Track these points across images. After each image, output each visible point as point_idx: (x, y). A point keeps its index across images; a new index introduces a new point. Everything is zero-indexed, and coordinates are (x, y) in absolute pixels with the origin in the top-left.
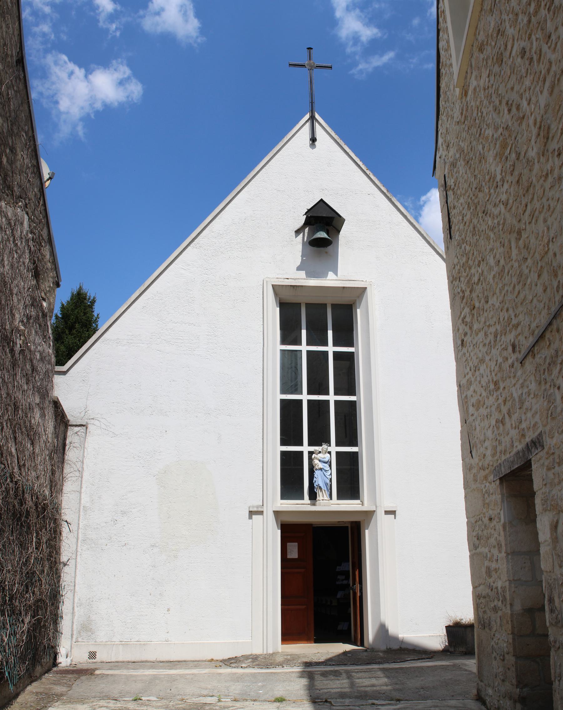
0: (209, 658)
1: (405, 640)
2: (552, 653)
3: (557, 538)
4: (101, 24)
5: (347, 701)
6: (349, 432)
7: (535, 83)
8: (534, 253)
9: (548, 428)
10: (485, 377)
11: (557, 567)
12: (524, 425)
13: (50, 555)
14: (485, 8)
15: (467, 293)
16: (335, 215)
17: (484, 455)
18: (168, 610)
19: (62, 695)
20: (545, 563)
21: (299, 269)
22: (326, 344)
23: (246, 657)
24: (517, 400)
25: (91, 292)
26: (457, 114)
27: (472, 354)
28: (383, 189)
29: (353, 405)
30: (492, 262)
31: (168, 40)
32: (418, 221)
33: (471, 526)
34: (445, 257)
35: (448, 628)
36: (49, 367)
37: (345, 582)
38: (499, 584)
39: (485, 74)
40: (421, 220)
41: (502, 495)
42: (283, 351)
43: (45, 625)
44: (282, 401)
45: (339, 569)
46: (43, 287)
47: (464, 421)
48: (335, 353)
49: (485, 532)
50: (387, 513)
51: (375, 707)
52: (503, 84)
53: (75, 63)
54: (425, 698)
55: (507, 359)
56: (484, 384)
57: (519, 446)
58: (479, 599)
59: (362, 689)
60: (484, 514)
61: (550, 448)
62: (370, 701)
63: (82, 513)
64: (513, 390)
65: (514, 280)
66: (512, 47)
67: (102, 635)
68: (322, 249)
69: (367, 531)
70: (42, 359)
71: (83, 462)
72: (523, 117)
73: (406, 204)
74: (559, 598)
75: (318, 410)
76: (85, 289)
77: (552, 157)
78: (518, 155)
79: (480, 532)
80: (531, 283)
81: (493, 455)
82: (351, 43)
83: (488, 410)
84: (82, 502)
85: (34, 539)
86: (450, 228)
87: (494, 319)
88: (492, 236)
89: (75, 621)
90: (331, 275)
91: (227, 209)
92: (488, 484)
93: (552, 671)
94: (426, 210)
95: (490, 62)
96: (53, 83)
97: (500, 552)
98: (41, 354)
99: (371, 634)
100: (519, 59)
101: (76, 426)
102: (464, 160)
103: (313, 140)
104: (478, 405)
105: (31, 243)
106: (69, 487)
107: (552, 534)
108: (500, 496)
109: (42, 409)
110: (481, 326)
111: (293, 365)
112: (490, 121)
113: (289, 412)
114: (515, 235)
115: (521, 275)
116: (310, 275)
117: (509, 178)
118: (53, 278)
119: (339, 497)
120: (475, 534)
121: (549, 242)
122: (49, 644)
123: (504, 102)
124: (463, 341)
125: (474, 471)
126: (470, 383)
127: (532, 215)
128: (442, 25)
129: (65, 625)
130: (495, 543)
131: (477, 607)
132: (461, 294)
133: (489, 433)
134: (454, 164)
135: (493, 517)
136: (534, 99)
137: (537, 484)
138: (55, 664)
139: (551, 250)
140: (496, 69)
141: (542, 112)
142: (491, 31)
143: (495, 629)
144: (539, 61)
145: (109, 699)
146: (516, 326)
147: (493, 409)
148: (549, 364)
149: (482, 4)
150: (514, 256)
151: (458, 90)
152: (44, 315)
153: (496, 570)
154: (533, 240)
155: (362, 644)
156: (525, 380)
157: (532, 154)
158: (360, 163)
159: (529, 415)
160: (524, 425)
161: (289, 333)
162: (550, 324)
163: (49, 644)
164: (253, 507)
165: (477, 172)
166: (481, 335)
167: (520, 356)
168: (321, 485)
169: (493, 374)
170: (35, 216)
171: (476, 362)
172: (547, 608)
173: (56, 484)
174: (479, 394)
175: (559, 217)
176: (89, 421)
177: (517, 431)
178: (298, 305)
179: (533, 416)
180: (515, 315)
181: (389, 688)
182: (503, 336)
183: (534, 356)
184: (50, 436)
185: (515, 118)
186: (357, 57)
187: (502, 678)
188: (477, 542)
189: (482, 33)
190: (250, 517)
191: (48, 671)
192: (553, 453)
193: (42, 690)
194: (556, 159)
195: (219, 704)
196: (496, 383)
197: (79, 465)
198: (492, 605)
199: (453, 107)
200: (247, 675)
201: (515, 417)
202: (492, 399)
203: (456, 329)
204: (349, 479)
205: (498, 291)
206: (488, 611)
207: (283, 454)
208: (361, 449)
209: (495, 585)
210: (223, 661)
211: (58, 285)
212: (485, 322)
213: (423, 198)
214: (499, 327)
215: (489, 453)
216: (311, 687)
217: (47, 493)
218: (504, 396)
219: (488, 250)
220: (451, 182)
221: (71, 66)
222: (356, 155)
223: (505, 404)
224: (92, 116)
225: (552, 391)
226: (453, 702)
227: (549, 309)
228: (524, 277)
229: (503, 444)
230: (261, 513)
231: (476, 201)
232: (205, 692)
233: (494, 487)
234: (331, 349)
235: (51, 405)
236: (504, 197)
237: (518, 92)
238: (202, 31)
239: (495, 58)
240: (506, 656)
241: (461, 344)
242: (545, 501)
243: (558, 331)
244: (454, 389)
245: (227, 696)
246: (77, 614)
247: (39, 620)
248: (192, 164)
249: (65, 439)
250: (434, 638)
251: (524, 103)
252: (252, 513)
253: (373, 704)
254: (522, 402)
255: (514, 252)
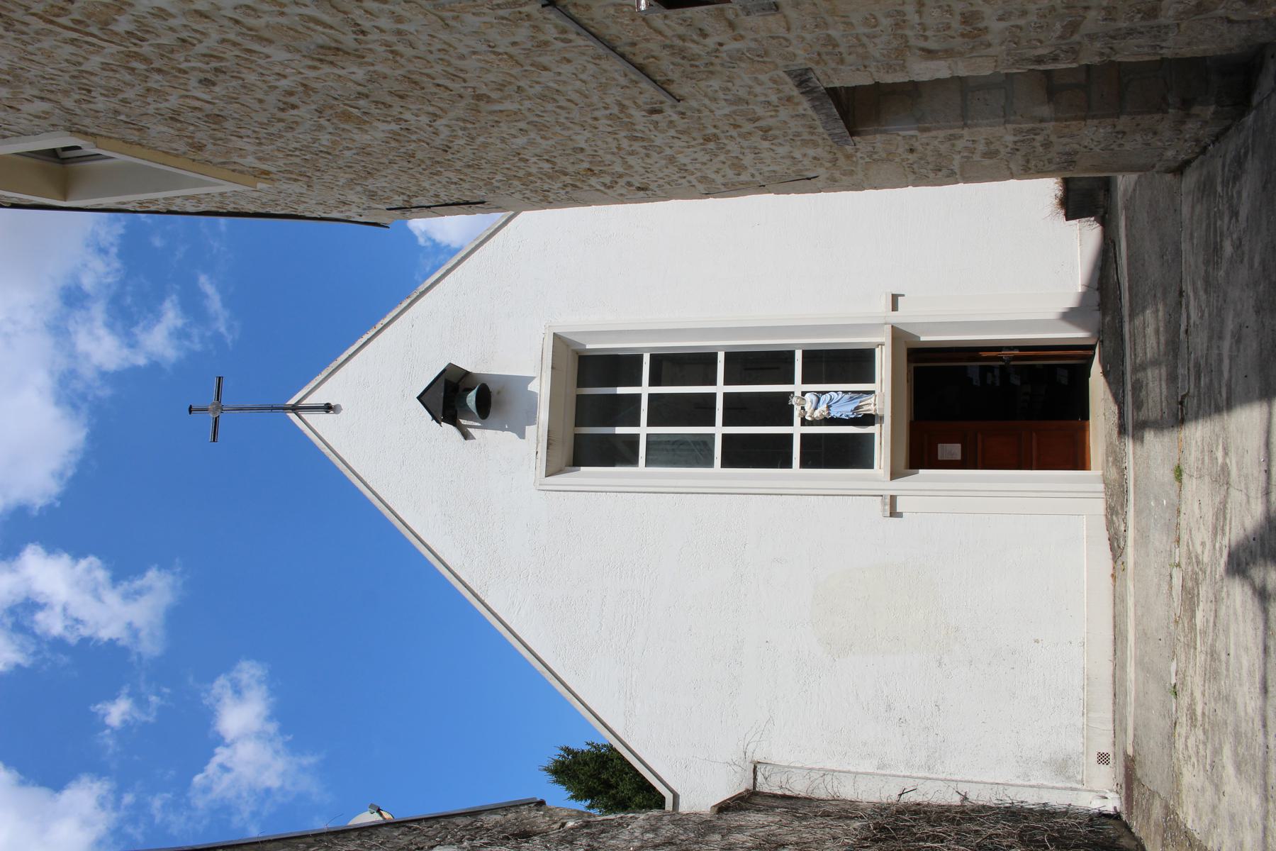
0: (1111, 580)
1: (1085, 282)
2: (1118, 58)
3: (946, 51)
4: (151, 719)
5: (1182, 371)
6: (772, 364)
7: (253, 66)
8: (512, 75)
9: (780, 62)
10: (696, 156)
11: (991, 51)
12: (774, 98)
13: (952, 821)
14: (136, 139)
15: (568, 180)
16: (442, 378)
17: (815, 158)
18: (1037, 641)
19: (1167, 807)
20: (984, 68)
21: (522, 435)
22: (638, 397)
23: (1110, 524)
24: (735, 108)
25: (553, 754)
26: (296, 188)
27: (661, 175)
28: (405, 304)
29: (730, 357)
30: (521, 141)
31: (176, 619)
32: (457, 251)
33: (920, 179)
34: (511, 213)
35: (1068, 217)
36: (666, 819)
37: (997, 372)
38: (1010, 138)
39: (239, 143)
40: (455, 245)
41: (875, 132)
42: (648, 463)
43: (1058, 831)
44: (724, 465)
45: (976, 382)
46: (543, 827)
47: (761, 188)
48: (652, 384)
49: (930, 159)
50: (895, 307)
51: (1192, 329)
52: (253, 115)
53: (207, 763)
54: (1178, 252)
55: (671, 122)
56: (707, 157)
57: (805, 105)
58: (1029, 170)
59: (1162, 347)
60: (903, 160)
61: (810, 59)
62: (1182, 335)
63: (888, 772)
64: (718, 113)
65: (550, 107)
66: (198, 99)
67: (1074, 744)
68: (493, 399)
69: (923, 339)
70: (654, 830)
71: (811, 769)
72: (304, 85)
73: (428, 269)
74: (1035, 48)
75: (738, 409)
76: (548, 762)
77: (366, 43)
78: (361, 95)
79: (930, 167)
80: (556, 82)
81: (816, 145)
82: (187, 343)
83: (747, 151)
84: (871, 771)
85: (929, 844)
86: (467, 203)
87: (610, 140)
88: (481, 139)
89: (1051, 785)
90: (533, 387)
91: (428, 543)
92: (859, 154)
93: (1146, 58)
94: (439, 237)
95: (220, 135)
96: (239, 796)
97: (961, 137)
98: (647, 831)
99: (1076, 334)
100: (217, 89)
101: (755, 779)
102: (366, 178)
103: (328, 408)
104: (738, 167)
105: (477, 843)
106: (848, 791)
107: (940, 59)
108: (878, 136)
109: (730, 830)
110: (619, 161)
111: (669, 447)
112: (308, 137)
113: (741, 454)
114: (482, 104)
115: (543, 97)
116: (532, 419)
117: (395, 111)
118: (530, 810)
119: (870, 379)
120: (932, 175)
121: (494, 53)
122: (1087, 825)
123: (281, 115)
124: (639, 189)
125: (837, 174)
126: (704, 179)
127: (453, 77)
128: (161, 207)
129: (1057, 800)
130: (948, 144)
131: (1041, 173)
132: (569, 189)
133: (782, 151)
134: (372, 195)
135: (907, 147)
136: (277, 69)
137: (863, 79)
138: (1116, 817)
139: (508, 50)
140: (230, 125)
141: (298, 57)
142: (172, 131)
143: (1076, 146)
144: (221, 59)
145: (1173, 734)
146: (622, 107)
147: (745, 144)
148: (684, 58)
149: (131, 143)
150: (514, 107)
151: (260, 186)
152: (587, 825)
153: (988, 143)
154: (491, 77)
155: (1092, 348)
156: (706, 95)
157: (360, 74)
158: (366, 337)
159: (758, 89)
160: (774, 98)
161: (622, 453)
162: (622, 56)
163: (1087, 825)
164: (884, 510)
165: (385, 160)
166: (631, 160)
167: (669, 101)
168: (852, 407)
169: (693, 143)
170: (436, 836)
171: (672, 169)
172: (1050, 67)
173: (845, 811)
174: (721, 166)
175: (457, 36)
176: (749, 759)
177: (781, 108)
178: (578, 438)
179: (761, 84)
180: (606, 108)
181: (1161, 307)
182: (637, 127)
183: (670, 81)
184: (770, 819)
185: (305, 99)
186: (208, 334)
187: (1151, 135)
188: (945, 171)
189: (174, 145)
190: (900, 515)
191: (1127, 827)
192: (819, 54)
193: (1159, 838)
194: (370, 37)
195: (1183, 566)
196: (707, 139)
197: (814, 775)
198: (1041, 149)
199: (287, 193)
200: (1137, 523)
201: (760, 111)
202: (732, 146)
203: (622, 199)
204: (846, 364)
205: (566, 133)
206: (1049, 156)
207: (804, 464)
208: (798, 346)
209: (1011, 145)
210: (1115, 559)
211: (542, 803)
212: (613, 153)
213: (422, 241)
214: (623, 134)
215: (811, 152)
216: (1158, 426)
217: (857, 824)
218: (727, 128)
219: (503, 146)
220: (398, 201)
221: (212, 768)
222: (353, 343)
223: (739, 126)
224: (289, 738)
225: (724, 55)
226: (1186, 210)
227: (599, 57)
228: (547, 93)
229: (800, 129)
230: (893, 499)
231: (428, 162)
232: (1165, 587)
233: (863, 144)
234: (645, 390)
235: (724, 817)
236: (424, 119)
237: (266, 93)
238: (165, 565)
239: (213, 126)
240: (1118, 129)
241: (644, 192)
242: (890, 68)
243: (634, 44)
244: (711, 202)
245: (1171, 553)
246: (1041, 781)
247: (1052, 839)
248: (358, 597)
249: (775, 796)
250: (1082, 239)
251: (284, 83)
252: (894, 513)
253: (1187, 331)
254: (739, 100)
255: (508, 106)
